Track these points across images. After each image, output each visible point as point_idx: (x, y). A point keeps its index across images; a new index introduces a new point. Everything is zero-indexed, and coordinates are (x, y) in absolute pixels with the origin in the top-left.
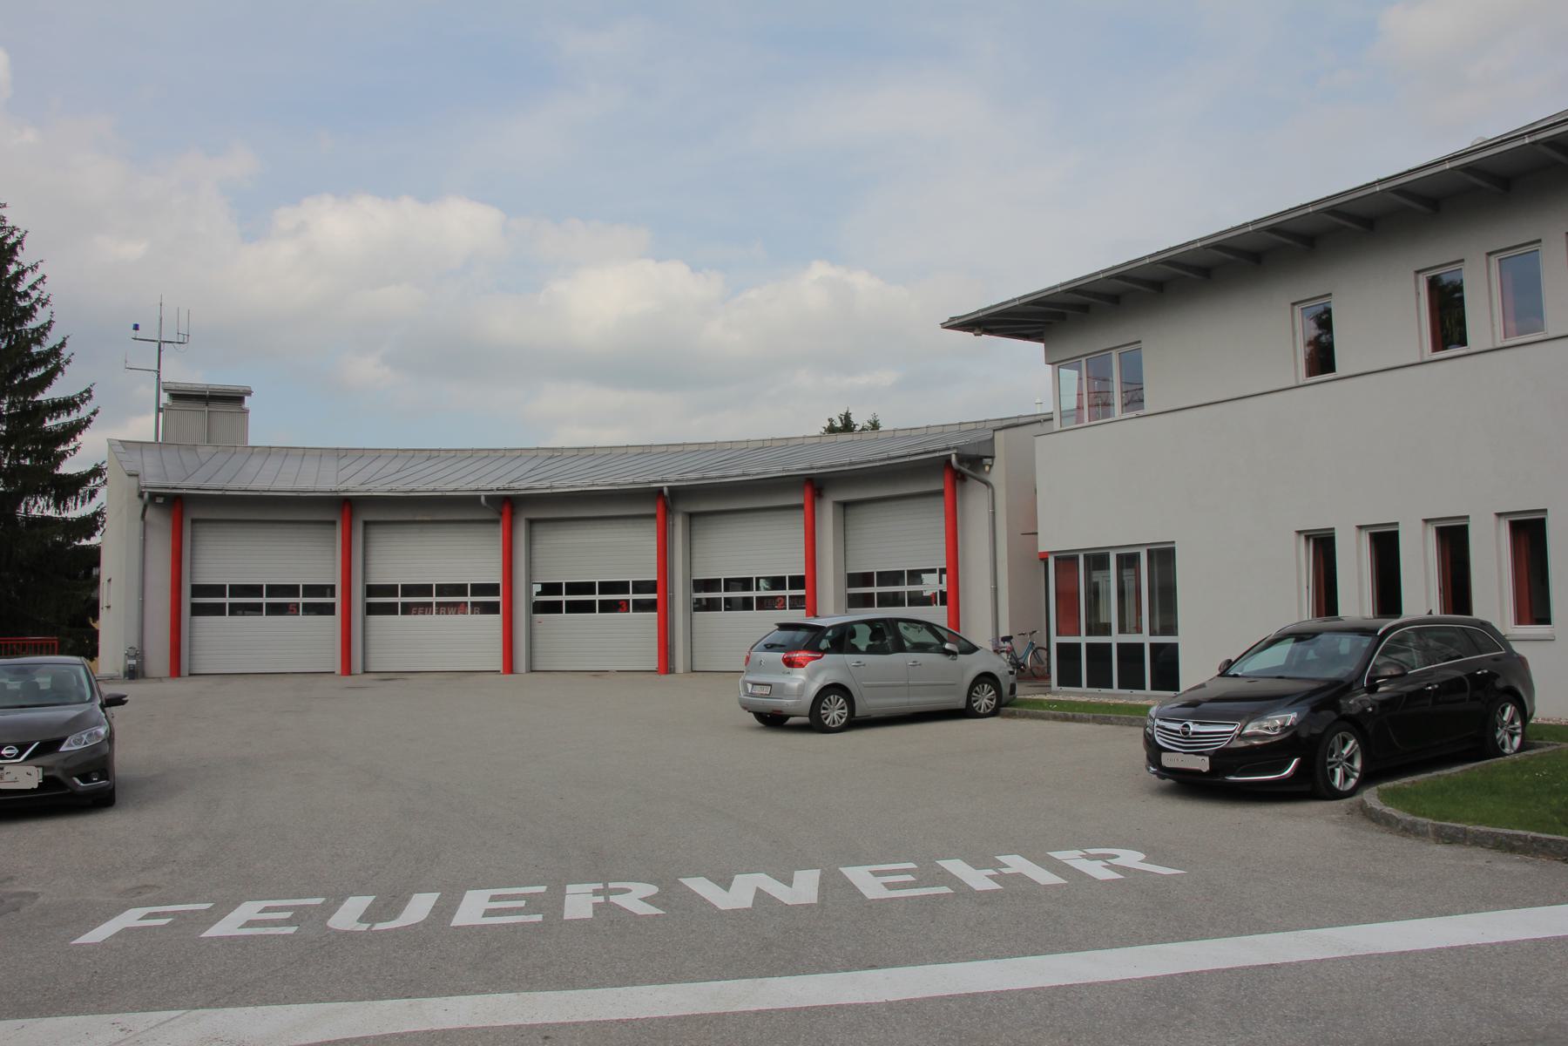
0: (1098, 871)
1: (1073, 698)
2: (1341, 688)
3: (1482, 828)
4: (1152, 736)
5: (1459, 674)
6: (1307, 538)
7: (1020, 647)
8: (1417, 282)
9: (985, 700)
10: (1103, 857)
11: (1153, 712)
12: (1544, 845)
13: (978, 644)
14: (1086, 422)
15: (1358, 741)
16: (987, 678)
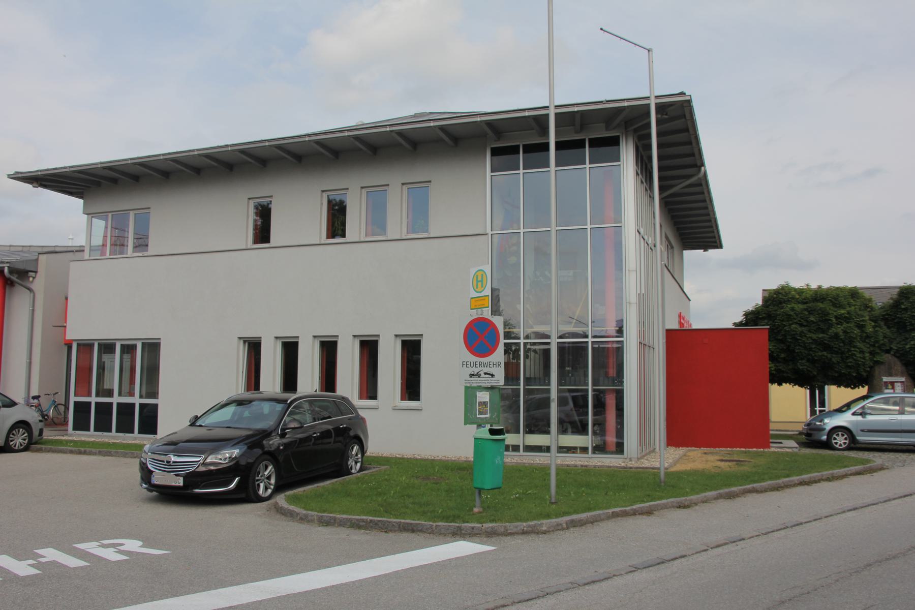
0: (111, 555)
1: (83, 439)
2: (266, 434)
3: (344, 516)
4: (145, 464)
5: (330, 427)
6: (245, 342)
7: (45, 403)
8: (322, 196)
9: (19, 439)
10: (113, 546)
11: (146, 448)
12: (376, 524)
13: (17, 401)
14: (108, 256)
15: (274, 467)
16: (23, 424)
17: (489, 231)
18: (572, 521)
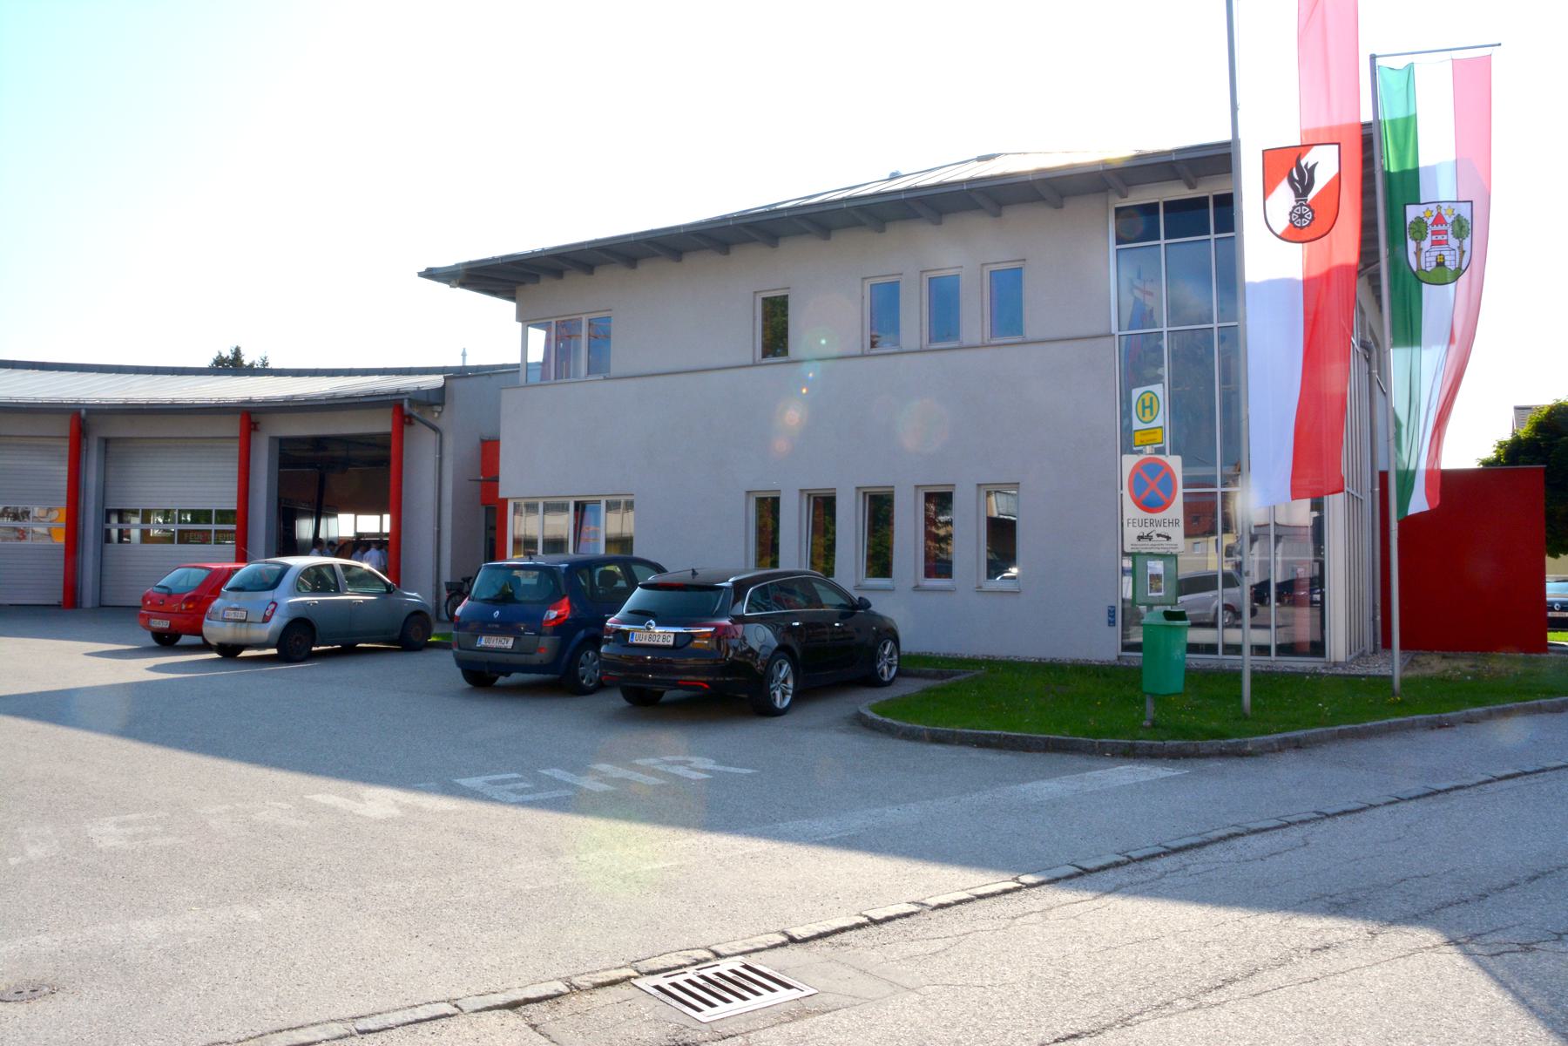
17: (1114, 329)
18: (1286, 740)
